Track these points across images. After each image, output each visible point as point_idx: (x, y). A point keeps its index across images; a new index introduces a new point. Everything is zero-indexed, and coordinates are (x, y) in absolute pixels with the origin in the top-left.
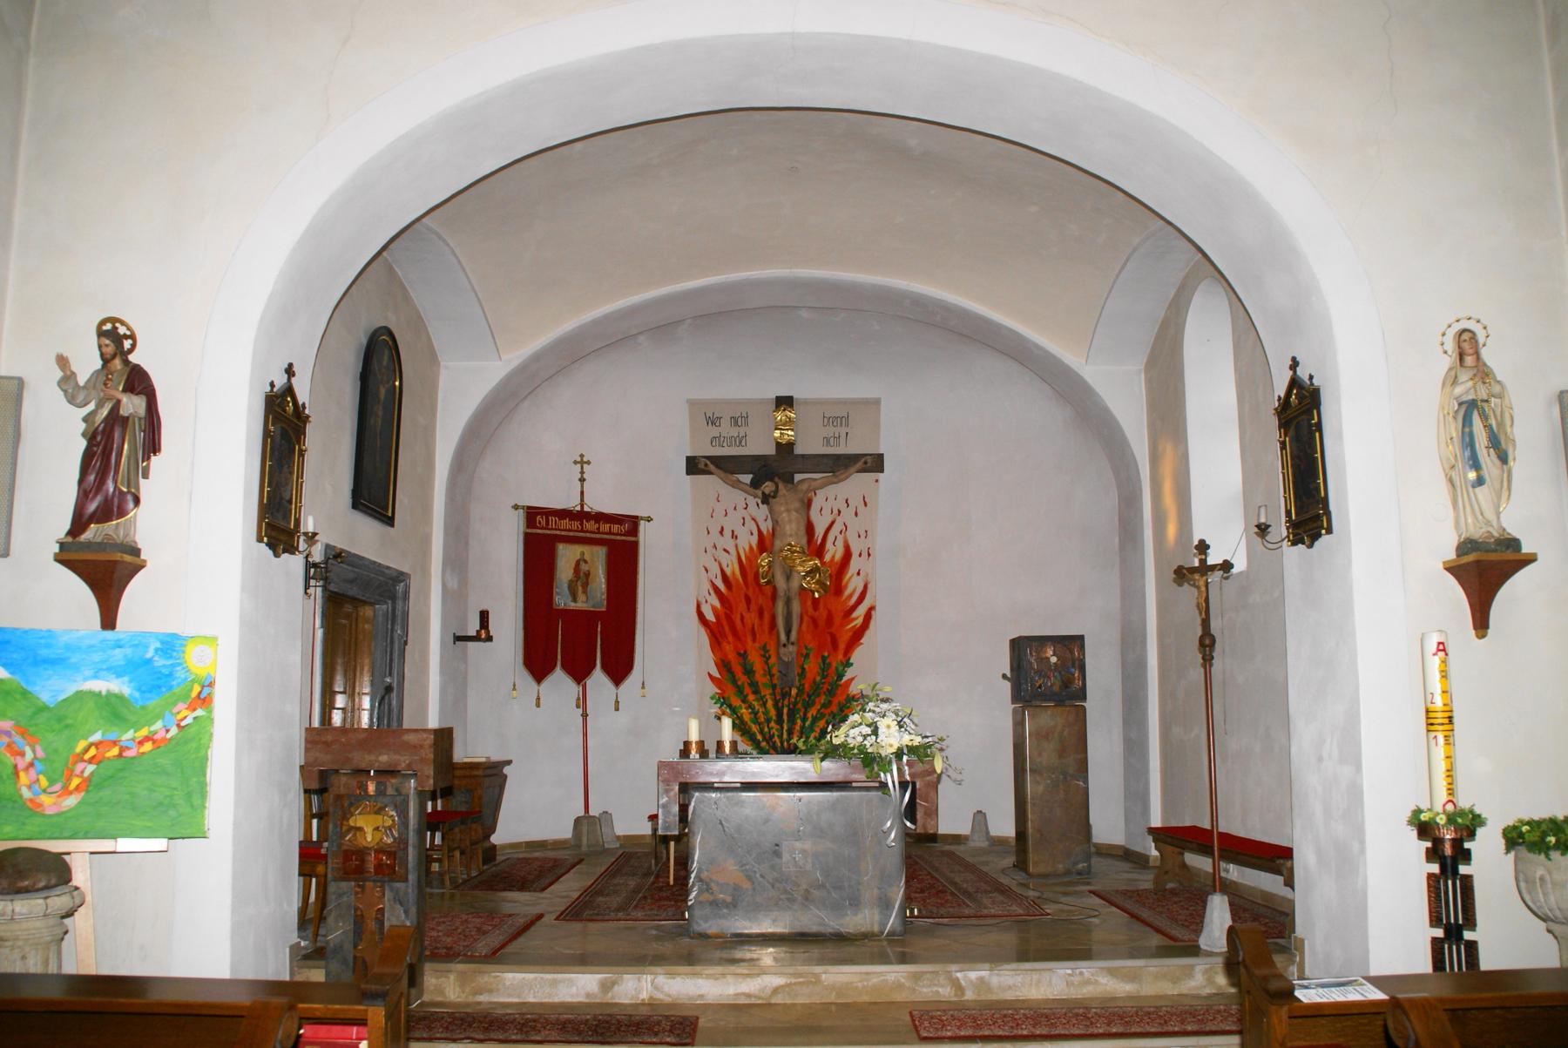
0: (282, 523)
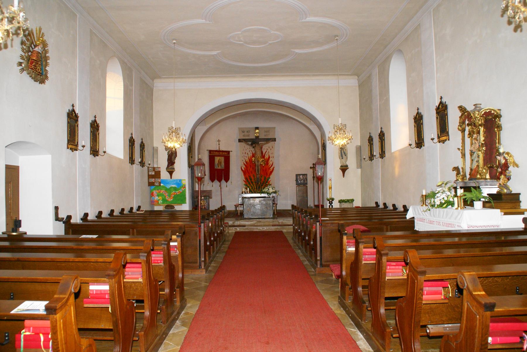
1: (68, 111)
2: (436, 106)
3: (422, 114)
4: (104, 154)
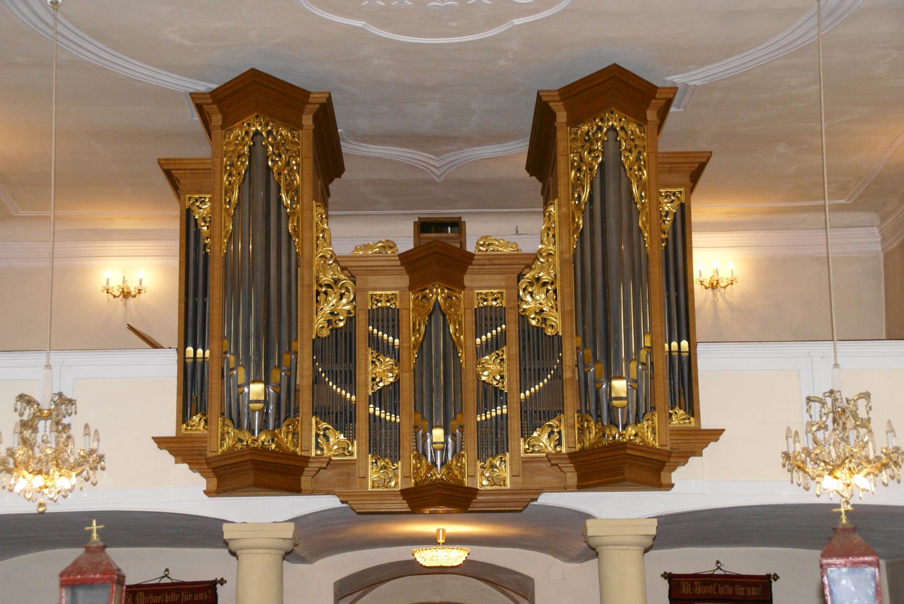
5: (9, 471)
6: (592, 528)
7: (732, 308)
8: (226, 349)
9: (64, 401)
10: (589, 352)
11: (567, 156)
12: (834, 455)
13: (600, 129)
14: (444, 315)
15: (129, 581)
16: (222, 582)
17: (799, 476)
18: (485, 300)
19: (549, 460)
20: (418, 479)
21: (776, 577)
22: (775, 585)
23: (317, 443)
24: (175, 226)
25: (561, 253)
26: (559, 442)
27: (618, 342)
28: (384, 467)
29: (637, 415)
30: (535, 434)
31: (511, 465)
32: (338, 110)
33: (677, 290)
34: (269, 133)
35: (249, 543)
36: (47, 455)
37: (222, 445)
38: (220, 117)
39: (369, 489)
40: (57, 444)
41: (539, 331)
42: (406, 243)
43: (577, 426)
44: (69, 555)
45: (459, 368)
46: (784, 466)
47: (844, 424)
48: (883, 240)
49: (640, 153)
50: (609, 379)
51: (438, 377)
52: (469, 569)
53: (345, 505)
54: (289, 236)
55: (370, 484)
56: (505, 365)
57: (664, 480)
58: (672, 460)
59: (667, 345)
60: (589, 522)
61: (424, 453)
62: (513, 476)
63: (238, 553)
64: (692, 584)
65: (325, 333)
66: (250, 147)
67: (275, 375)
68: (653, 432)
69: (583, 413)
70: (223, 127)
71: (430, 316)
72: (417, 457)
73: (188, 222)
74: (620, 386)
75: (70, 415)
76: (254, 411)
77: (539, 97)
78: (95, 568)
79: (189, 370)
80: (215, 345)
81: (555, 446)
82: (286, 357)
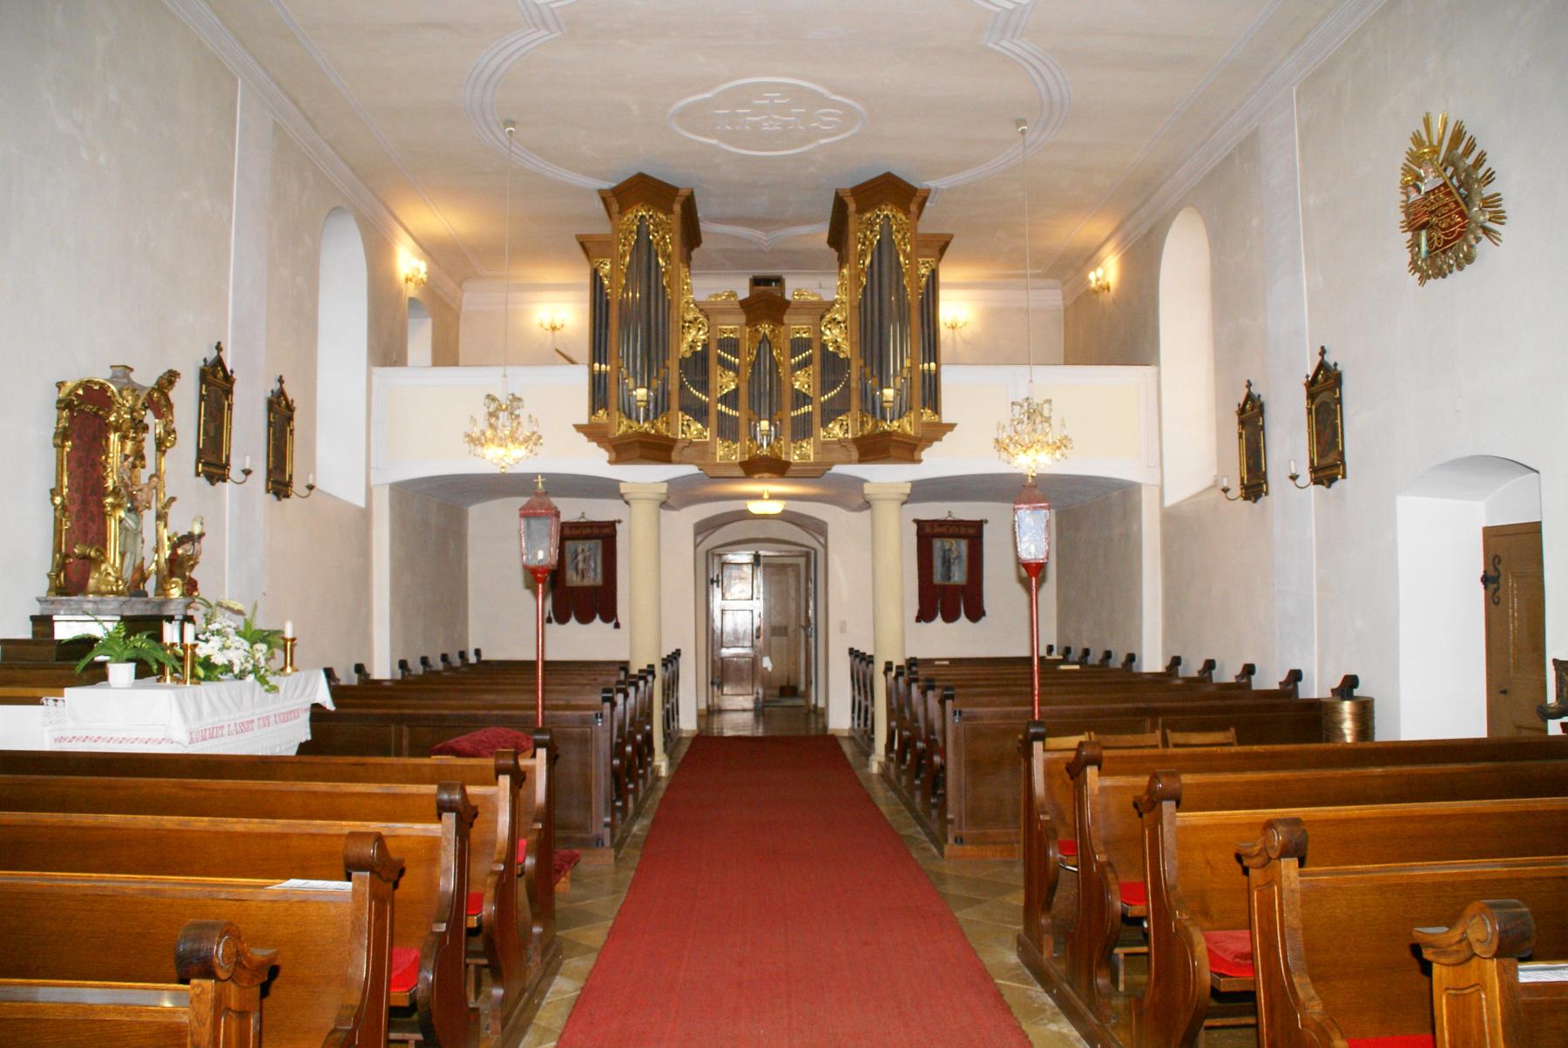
0: (280, 479)
1: (202, 364)
2: (1307, 376)
3: (1262, 399)
4: (307, 491)
5: (482, 445)
6: (867, 489)
7: (966, 342)
8: (621, 364)
9: (516, 399)
10: (868, 370)
11: (856, 234)
12: (1027, 441)
13: (878, 216)
14: (770, 344)
15: (563, 518)
16: (620, 522)
17: (1004, 455)
18: (798, 333)
19: (840, 443)
20: (751, 455)
21: (986, 521)
22: (986, 528)
23: (683, 430)
24: (586, 280)
25: (851, 301)
26: (847, 431)
27: (889, 363)
28: (728, 447)
29: (900, 413)
30: (831, 425)
31: (814, 446)
32: (697, 200)
33: (929, 328)
34: (651, 217)
35: (638, 496)
36: (505, 435)
37: (619, 430)
38: (617, 205)
39: (718, 461)
40: (512, 427)
41: (835, 355)
42: (744, 293)
43: (859, 420)
44: (523, 501)
45: (779, 379)
46: (995, 447)
47: (1035, 420)
48: (1064, 299)
49: (905, 233)
50: (881, 388)
51: (765, 385)
52: (786, 517)
53: (701, 472)
54: (664, 288)
55: (718, 457)
56: (811, 378)
57: (916, 457)
58: (923, 443)
59: (921, 366)
60: (866, 485)
61: (755, 438)
62: (815, 453)
63: (630, 502)
64: (932, 526)
65: (688, 355)
66: (638, 227)
67: (655, 383)
68: (911, 425)
69: (863, 412)
70: (620, 212)
71: (760, 343)
72: (750, 440)
73: (596, 278)
74: (889, 393)
75: (519, 408)
76: (640, 408)
77: (837, 193)
78: (541, 505)
79: (597, 378)
80: (614, 362)
81: (844, 434)
82: (662, 371)
